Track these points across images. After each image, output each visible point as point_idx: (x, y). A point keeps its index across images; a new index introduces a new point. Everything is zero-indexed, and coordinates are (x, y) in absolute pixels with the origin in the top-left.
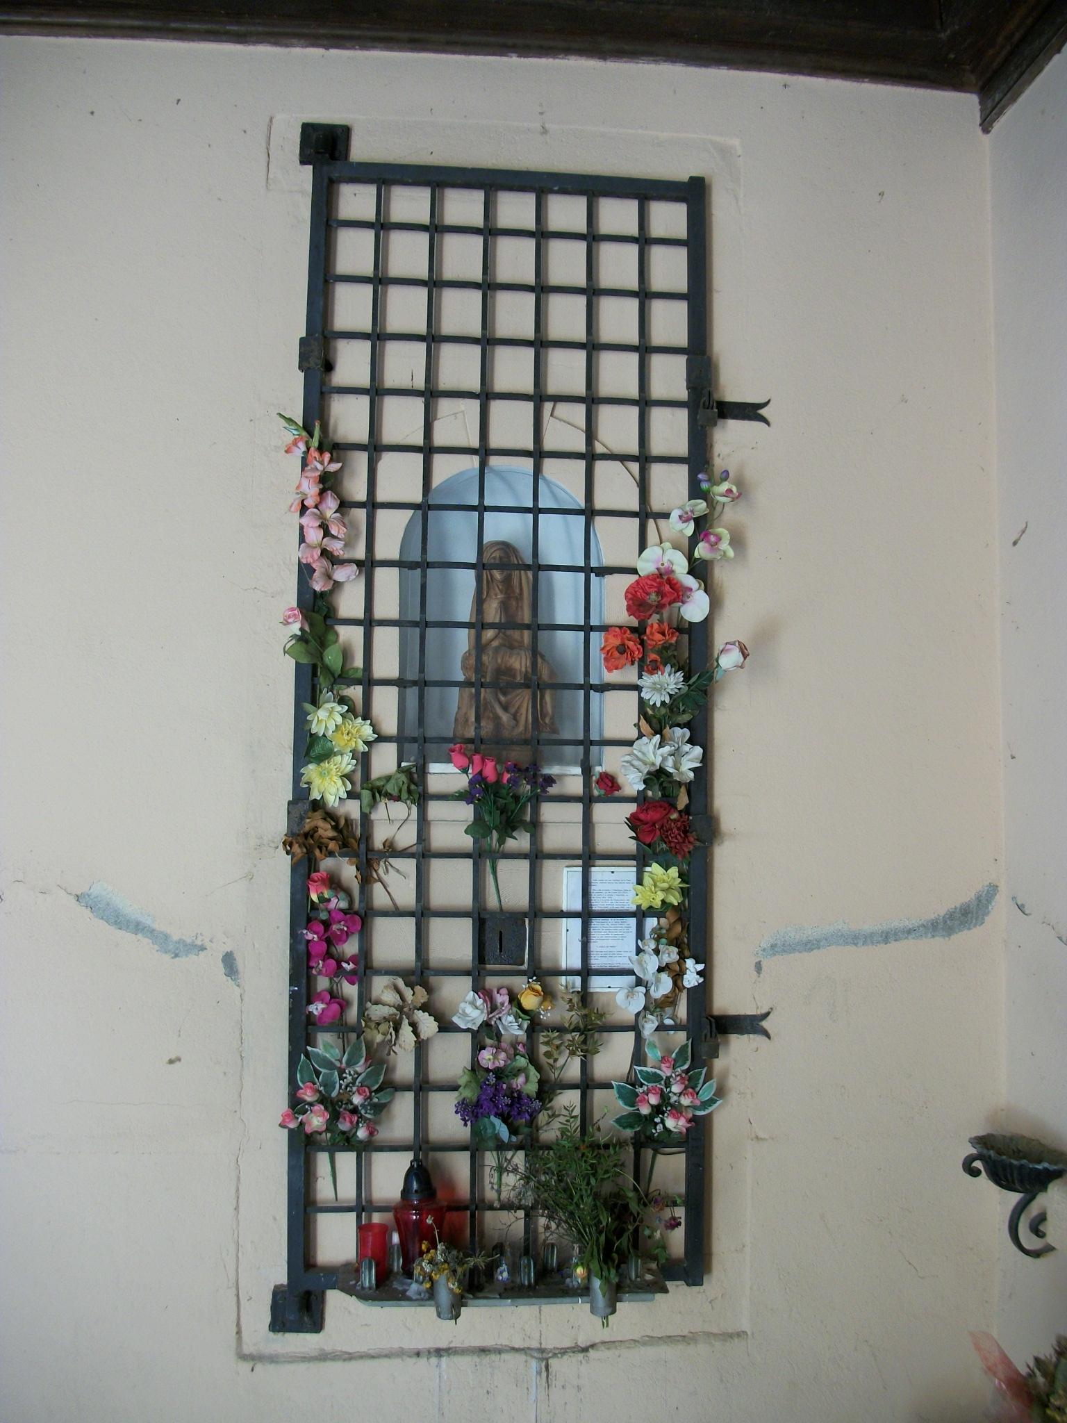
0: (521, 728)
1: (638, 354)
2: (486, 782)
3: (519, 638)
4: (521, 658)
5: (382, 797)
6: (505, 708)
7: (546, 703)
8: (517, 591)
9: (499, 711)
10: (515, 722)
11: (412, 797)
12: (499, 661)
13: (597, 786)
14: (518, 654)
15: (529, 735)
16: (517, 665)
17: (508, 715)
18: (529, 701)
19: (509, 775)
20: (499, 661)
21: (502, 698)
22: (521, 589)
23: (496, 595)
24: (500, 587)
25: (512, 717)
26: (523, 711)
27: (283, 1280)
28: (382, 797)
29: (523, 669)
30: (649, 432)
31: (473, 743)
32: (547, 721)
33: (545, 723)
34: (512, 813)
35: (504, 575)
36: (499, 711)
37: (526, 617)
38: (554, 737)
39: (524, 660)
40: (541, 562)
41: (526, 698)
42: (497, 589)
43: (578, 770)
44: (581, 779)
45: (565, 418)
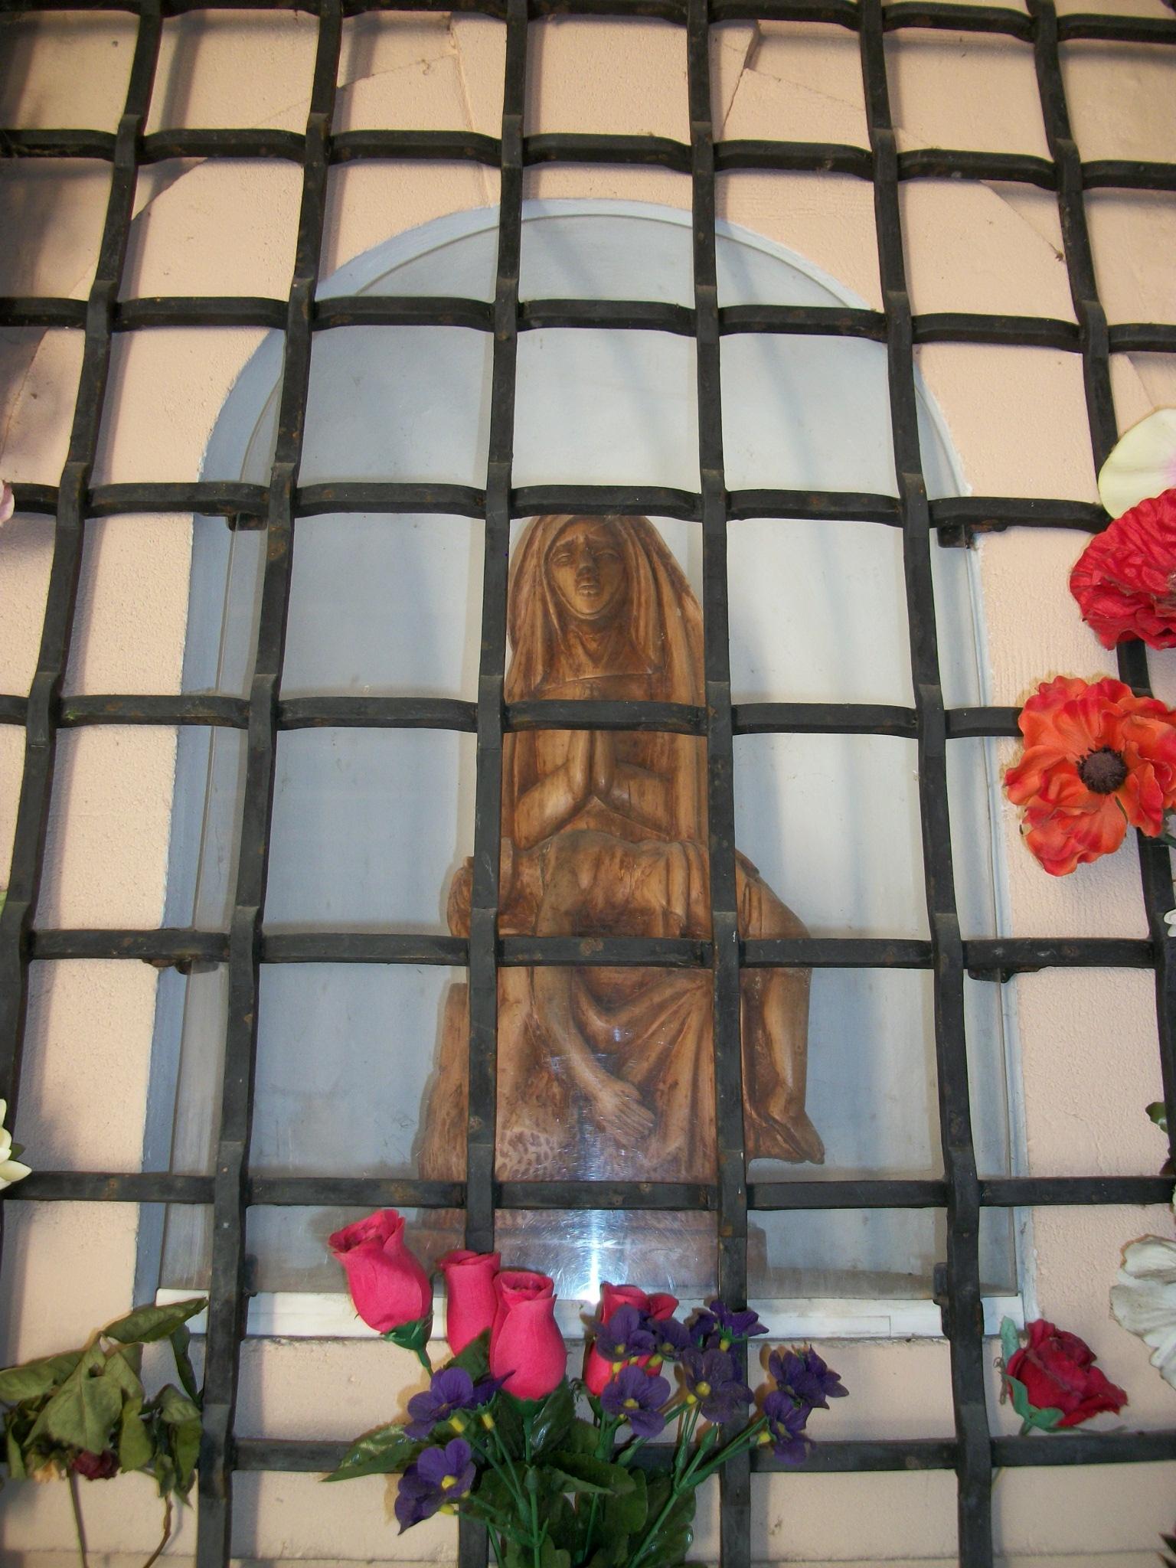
0: (676, 1142)
1: (873, 184)
2: (507, 1400)
3: (660, 813)
4: (668, 868)
5: (33, 1457)
6: (613, 1062)
7: (769, 1042)
8: (653, 655)
9: (587, 1072)
10: (649, 1115)
11: (167, 1460)
12: (585, 880)
13: (1020, 1388)
14: (657, 854)
15: (703, 1170)
16: (653, 895)
17: (619, 1086)
18: (700, 1039)
19: (617, 1367)
20: (585, 880)
21: (597, 1023)
22: (665, 649)
23: (578, 670)
24: (593, 646)
25: (635, 1093)
26: (683, 1072)
27: (472, 855)
28: (33, 1457)
29: (679, 909)
30: (910, 274)
31: (461, 1204)
32: (776, 1111)
33: (768, 1118)
34: (656, 1313)
35: (606, 597)
36: (587, 1072)
37: (685, 688)
38: (806, 1170)
39: (678, 876)
40: (741, 689)
41: (694, 1021)
42: (580, 651)
43: (927, 1316)
44: (943, 1352)
45: (417, 254)
